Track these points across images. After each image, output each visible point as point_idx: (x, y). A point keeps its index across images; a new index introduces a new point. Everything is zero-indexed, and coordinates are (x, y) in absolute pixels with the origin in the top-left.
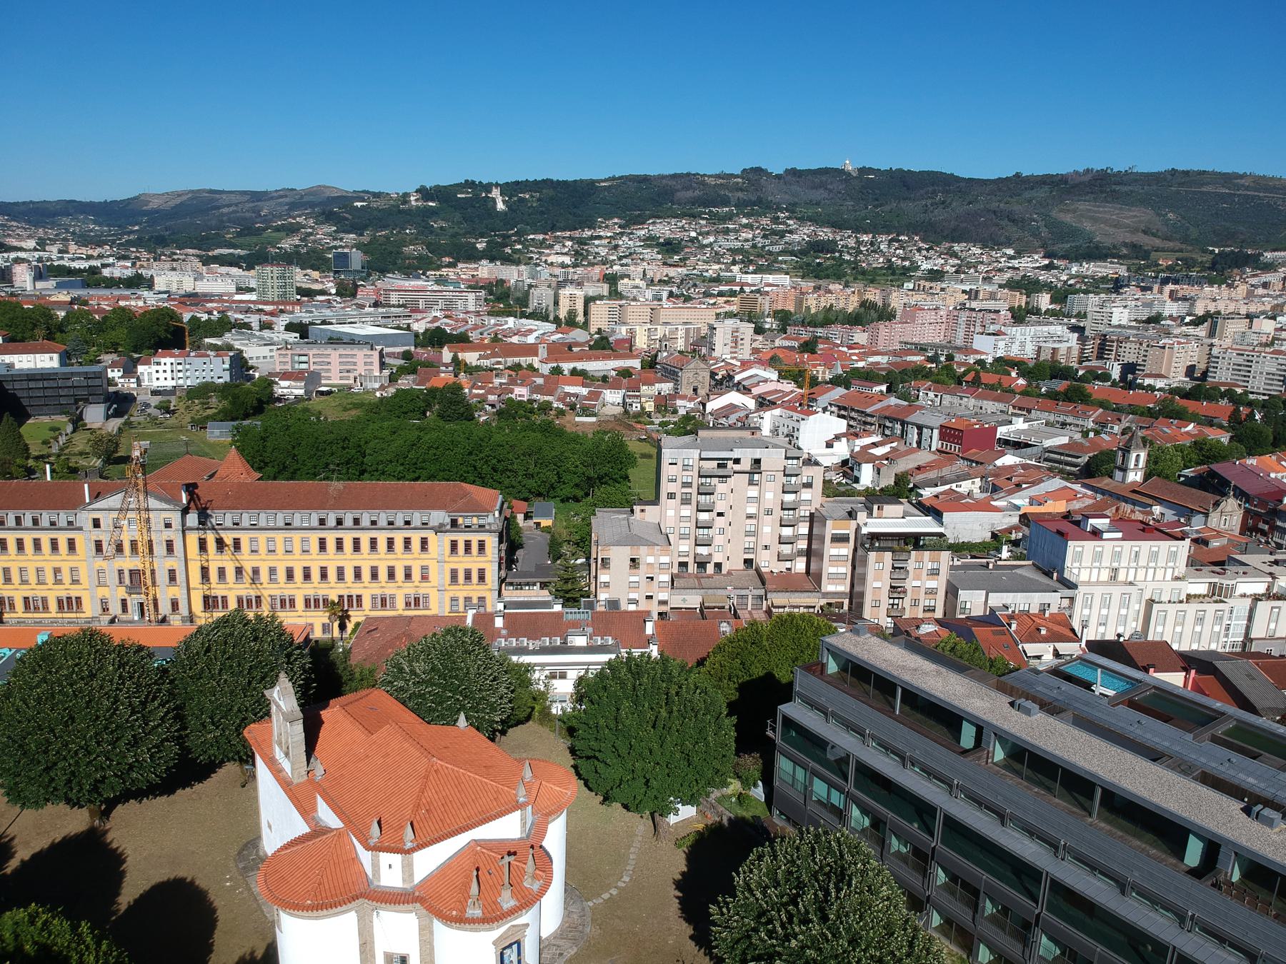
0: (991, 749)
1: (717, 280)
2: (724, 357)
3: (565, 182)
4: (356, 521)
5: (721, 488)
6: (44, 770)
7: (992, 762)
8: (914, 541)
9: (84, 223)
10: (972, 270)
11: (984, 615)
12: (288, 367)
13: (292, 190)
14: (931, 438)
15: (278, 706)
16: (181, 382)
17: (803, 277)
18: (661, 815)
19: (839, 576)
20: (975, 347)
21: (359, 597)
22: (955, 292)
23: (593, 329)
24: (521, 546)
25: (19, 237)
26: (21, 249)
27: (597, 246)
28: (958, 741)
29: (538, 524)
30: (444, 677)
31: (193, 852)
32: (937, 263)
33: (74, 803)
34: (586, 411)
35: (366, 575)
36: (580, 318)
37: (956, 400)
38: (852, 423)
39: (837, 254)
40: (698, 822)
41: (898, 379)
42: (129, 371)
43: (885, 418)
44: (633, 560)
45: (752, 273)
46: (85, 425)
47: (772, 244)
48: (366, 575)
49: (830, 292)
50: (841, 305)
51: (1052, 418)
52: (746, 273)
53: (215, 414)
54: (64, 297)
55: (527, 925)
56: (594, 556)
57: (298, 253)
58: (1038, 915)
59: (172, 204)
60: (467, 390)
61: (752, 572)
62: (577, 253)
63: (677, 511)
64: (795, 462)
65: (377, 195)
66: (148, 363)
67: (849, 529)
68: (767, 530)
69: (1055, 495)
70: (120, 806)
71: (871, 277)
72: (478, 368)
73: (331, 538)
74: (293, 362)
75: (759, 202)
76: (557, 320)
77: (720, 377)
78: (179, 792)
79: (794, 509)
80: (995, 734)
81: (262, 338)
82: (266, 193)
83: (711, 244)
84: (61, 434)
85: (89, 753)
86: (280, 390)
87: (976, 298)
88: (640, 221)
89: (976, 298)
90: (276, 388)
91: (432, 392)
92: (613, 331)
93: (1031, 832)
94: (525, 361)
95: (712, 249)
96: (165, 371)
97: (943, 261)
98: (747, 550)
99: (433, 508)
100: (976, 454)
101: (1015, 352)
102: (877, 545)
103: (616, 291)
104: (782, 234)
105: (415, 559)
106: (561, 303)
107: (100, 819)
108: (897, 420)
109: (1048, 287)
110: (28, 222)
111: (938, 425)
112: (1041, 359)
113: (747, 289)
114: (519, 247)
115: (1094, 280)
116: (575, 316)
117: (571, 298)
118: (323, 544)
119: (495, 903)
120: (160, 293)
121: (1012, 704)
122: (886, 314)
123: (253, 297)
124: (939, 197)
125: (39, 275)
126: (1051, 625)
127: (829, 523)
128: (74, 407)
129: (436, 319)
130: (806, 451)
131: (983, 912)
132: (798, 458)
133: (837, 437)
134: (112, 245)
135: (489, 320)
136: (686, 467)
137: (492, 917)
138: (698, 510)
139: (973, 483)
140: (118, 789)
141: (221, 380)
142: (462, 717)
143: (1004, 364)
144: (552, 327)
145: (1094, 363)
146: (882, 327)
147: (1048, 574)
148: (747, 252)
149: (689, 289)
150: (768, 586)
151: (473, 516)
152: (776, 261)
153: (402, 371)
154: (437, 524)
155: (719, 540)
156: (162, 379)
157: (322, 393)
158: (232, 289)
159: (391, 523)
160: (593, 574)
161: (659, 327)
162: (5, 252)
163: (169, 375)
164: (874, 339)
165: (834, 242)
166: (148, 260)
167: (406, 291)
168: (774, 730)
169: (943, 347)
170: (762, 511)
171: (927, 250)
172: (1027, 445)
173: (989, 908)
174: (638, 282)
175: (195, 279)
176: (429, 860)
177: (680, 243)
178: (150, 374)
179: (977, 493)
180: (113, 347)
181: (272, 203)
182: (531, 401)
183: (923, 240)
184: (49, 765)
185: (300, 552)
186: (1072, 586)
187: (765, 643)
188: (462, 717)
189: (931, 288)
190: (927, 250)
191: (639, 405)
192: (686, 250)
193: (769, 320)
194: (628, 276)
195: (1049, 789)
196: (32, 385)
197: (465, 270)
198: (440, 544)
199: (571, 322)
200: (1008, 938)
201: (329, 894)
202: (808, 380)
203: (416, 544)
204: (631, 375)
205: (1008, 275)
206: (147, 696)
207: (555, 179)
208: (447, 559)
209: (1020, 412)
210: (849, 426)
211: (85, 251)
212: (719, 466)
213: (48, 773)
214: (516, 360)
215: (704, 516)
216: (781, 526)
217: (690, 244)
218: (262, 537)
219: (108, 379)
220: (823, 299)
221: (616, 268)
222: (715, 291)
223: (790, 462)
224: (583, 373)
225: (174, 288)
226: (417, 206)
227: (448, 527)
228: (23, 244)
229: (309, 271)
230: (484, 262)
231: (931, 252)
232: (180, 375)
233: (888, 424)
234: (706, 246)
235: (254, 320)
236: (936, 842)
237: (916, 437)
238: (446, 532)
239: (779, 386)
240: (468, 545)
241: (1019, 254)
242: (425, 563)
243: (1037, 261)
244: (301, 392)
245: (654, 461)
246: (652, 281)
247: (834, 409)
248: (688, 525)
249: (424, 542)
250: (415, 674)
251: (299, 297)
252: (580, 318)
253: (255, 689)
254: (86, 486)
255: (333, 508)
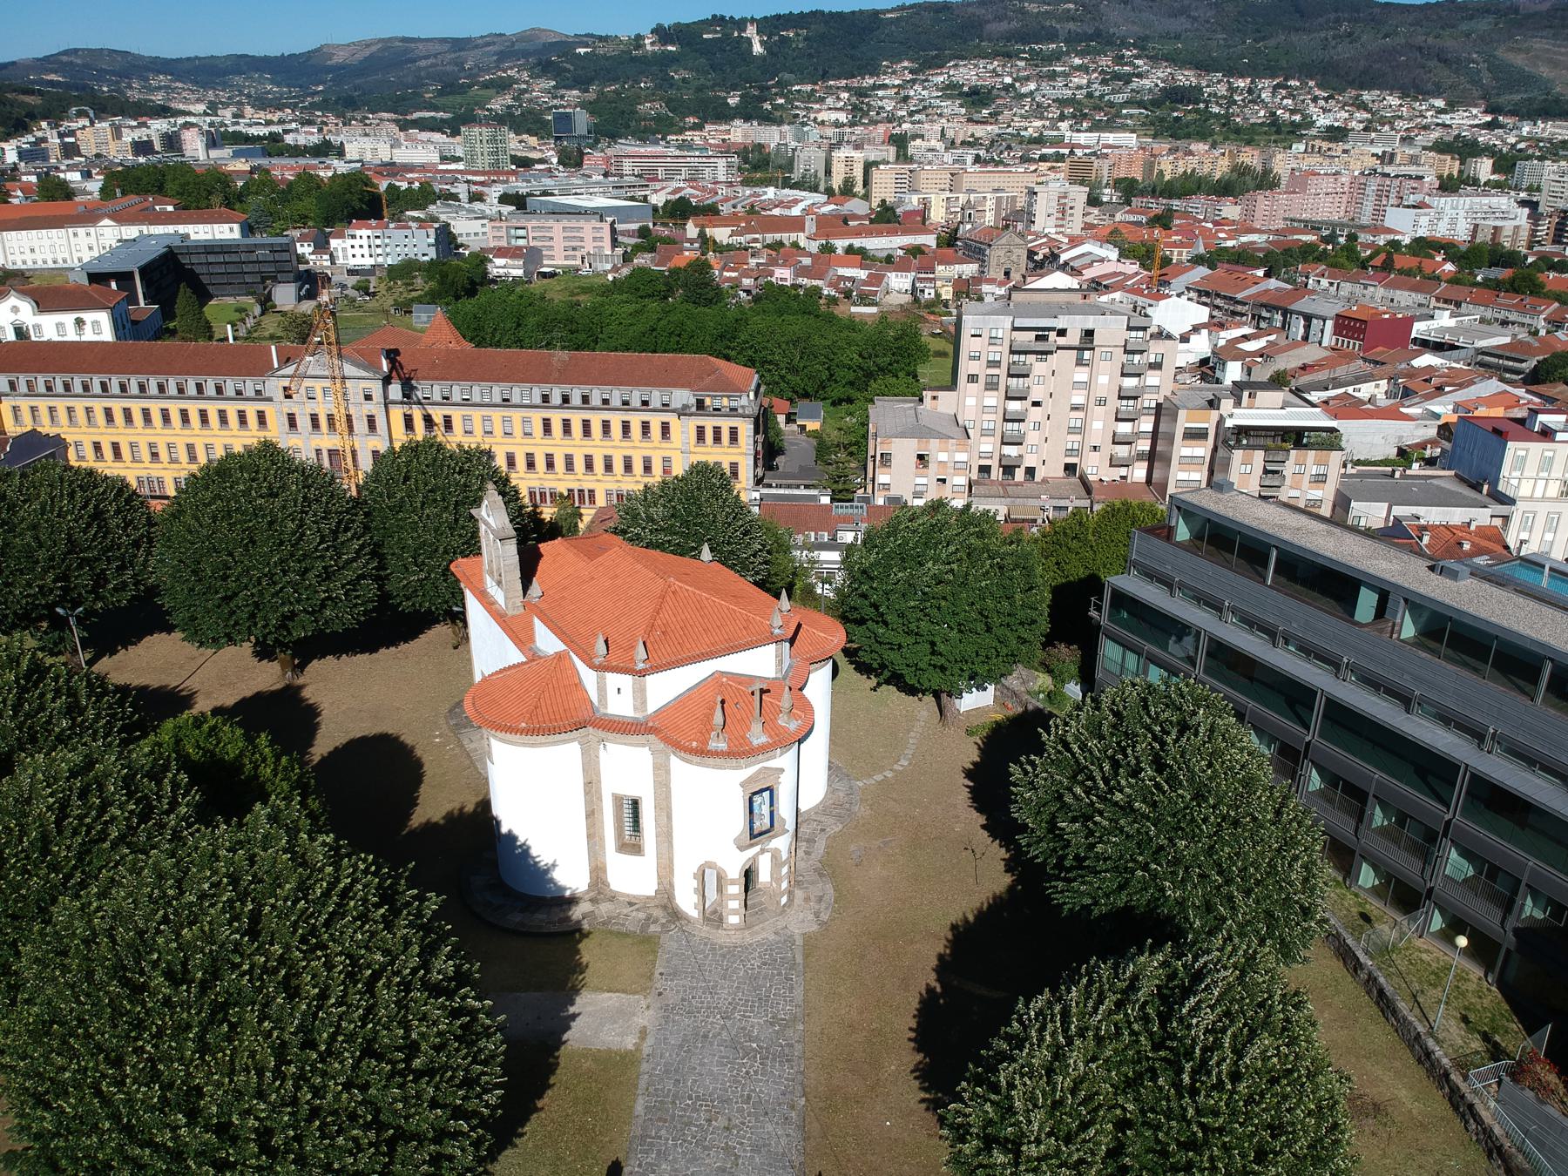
0: (1398, 621)
1: (1039, 141)
2: (1046, 231)
3: (840, 15)
4: (585, 399)
5: (1039, 367)
6: (223, 599)
7: (1398, 638)
8: (1295, 437)
9: (260, 83)
10: (1387, 128)
11: (1386, 528)
12: (504, 244)
13: (501, 35)
14: (1322, 331)
15: (487, 524)
16: (380, 260)
17: (1155, 137)
18: (950, 695)
19: (1195, 461)
20: (1387, 224)
21: (591, 492)
22: (1362, 155)
23: (875, 203)
24: (781, 451)
25: (186, 101)
26: (190, 114)
27: (881, 99)
28: (1352, 615)
29: (803, 428)
30: (686, 523)
31: (398, 709)
32: (1337, 118)
33: (264, 652)
34: (865, 299)
35: (599, 465)
36: (859, 188)
37: (1358, 289)
38: (1215, 313)
39: (1202, 106)
40: (996, 712)
41: (1278, 260)
42: (322, 246)
43: (1262, 305)
44: (921, 457)
45: (1086, 131)
46: (275, 306)
47: (1113, 92)
48: (599, 465)
49: (1191, 153)
50: (1206, 169)
51: (1489, 314)
52: (1078, 131)
53: (421, 296)
54: (242, 165)
55: (782, 770)
56: (871, 453)
57: (511, 115)
58: (1448, 823)
59: (360, 56)
60: (717, 273)
61: (1075, 480)
62: (855, 108)
63: (980, 399)
64: (1140, 334)
65: (601, 39)
66: (341, 236)
67: (1209, 421)
68: (1097, 425)
69: (1490, 401)
70: (315, 662)
71: (1247, 135)
72: (729, 247)
73: (557, 418)
74: (509, 236)
75: (1096, 35)
76: (829, 192)
77: (1040, 257)
78: (383, 651)
79: (1136, 398)
80: (1406, 600)
81: (470, 211)
82: (469, 40)
83: (1031, 93)
84: (248, 315)
85: (275, 583)
86: (495, 270)
87: (1391, 161)
88: (938, 63)
89: (1391, 161)
90: (489, 267)
91: (675, 272)
92: (901, 202)
93: (1446, 719)
94: (787, 237)
95: (1033, 99)
96: (361, 246)
97: (1347, 115)
98: (1070, 452)
99: (675, 386)
100: (1383, 352)
101: (1442, 231)
102: (1245, 442)
103: (905, 155)
104: (1127, 79)
105: (655, 448)
106: (834, 170)
107: (293, 671)
108: (1276, 308)
109: (1490, 151)
110: (195, 83)
111: (1333, 314)
112: (1478, 240)
113: (1079, 152)
114: (781, 101)
115: (1552, 144)
116: (853, 186)
117: (848, 162)
118: (547, 426)
119: (743, 737)
120: (351, 162)
121: (1432, 568)
122: (1266, 181)
123: (461, 166)
124: (1345, 27)
125: (213, 142)
126: (1477, 540)
127: (1182, 414)
128: (261, 286)
129: (679, 190)
130: (1155, 322)
131: (1370, 824)
132: (1144, 329)
133: (1196, 329)
134: (294, 107)
135: (744, 191)
136: (993, 341)
137: (739, 752)
138: (1008, 398)
139: (1377, 386)
140: (311, 628)
141: (426, 258)
142: (706, 548)
143: (1423, 246)
144: (820, 198)
145: (1549, 248)
146: (1260, 198)
147: (1477, 487)
148: (1079, 102)
149: (1001, 153)
150: (1095, 496)
151: (722, 396)
152: (1118, 115)
153: (637, 249)
154: (679, 406)
155: (1032, 438)
156: (359, 256)
157: (544, 275)
158: (435, 158)
159: (625, 403)
160: (870, 475)
161: (961, 195)
162: (172, 116)
163: (366, 251)
164: (1249, 213)
165: (1199, 89)
166: (337, 125)
167: (641, 157)
168: (1099, 609)
169: (1342, 225)
170: (1092, 400)
171: (1326, 99)
172: (1453, 347)
173: (1378, 818)
174: (934, 143)
175: (392, 147)
176: (667, 687)
177: (990, 92)
178: (344, 250)
179: (1382, 400)
180: (302, 220)
181: (478, 52)
182: (795, 286)
183: (1321, 86)
184: (229, 593)
185: (462, 432)
186: (1509, 501)
187: (1090, 537)
188: (706, 548)
189: (1329, 149)
190: (1326, 99)
191: (932, 291)
192: (999, 102)
193: (1107, 191)
194: (922, 137)
195: (1476, 670)
196: (211, 259)
197: (713, 133)
198: (683, 430)
199: (847, 190)
200: (1405, 854)
201: (547, 718)
202: (1158, 261)
203: (656, 430)
204: (923, 253)
205: (1435, 135)
206: (338, 526)
207: (827, 10)
208: (693, 449)
209: (1445, 306)
210: (1212, 317)
211: (262, 116)
212: (1038, 338)
213: (227, 604)
214: (778, 236)
215: (1014, 406)
216: (1117, 420)
217: (1003, 93)
218: (477, 414)
219: (298, 255)
220: (1181, 162)
221: (905, 126)
222: (1037, 154)
223: (1133, 334)
224: (862, 252)
225: (368, 157)
226: (653, 51)
227: (694, 409)
228: (192, 108)
229: (525, 136)
230: (737, 122)
231: (1332, 103)
232: (379, 251)
233: (1265, 314)
234: (1025, 96)
235: (461, 190)
236: (1312, 736)
237: (1302, 331)
238: (691, 415)
239: (1120, 268)
240: (717, 431)
241: (1451, 107)
242: (667, 454)
243: (1476, 116)
244: (520, 272)
245: (950, 361)
246: (953, 143)
247: (1193, 295)
248: (993, 417)
249: (665, 428)
250: (653, 520)
251: (514, 167)
252: (859, 188)
253: (463, 528)
254: (273, 348)
255: (558, 382)
